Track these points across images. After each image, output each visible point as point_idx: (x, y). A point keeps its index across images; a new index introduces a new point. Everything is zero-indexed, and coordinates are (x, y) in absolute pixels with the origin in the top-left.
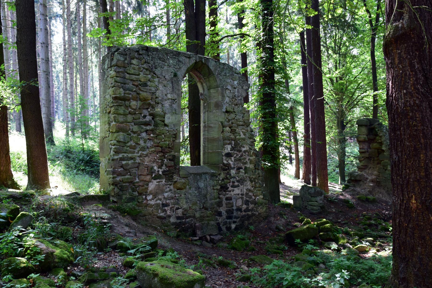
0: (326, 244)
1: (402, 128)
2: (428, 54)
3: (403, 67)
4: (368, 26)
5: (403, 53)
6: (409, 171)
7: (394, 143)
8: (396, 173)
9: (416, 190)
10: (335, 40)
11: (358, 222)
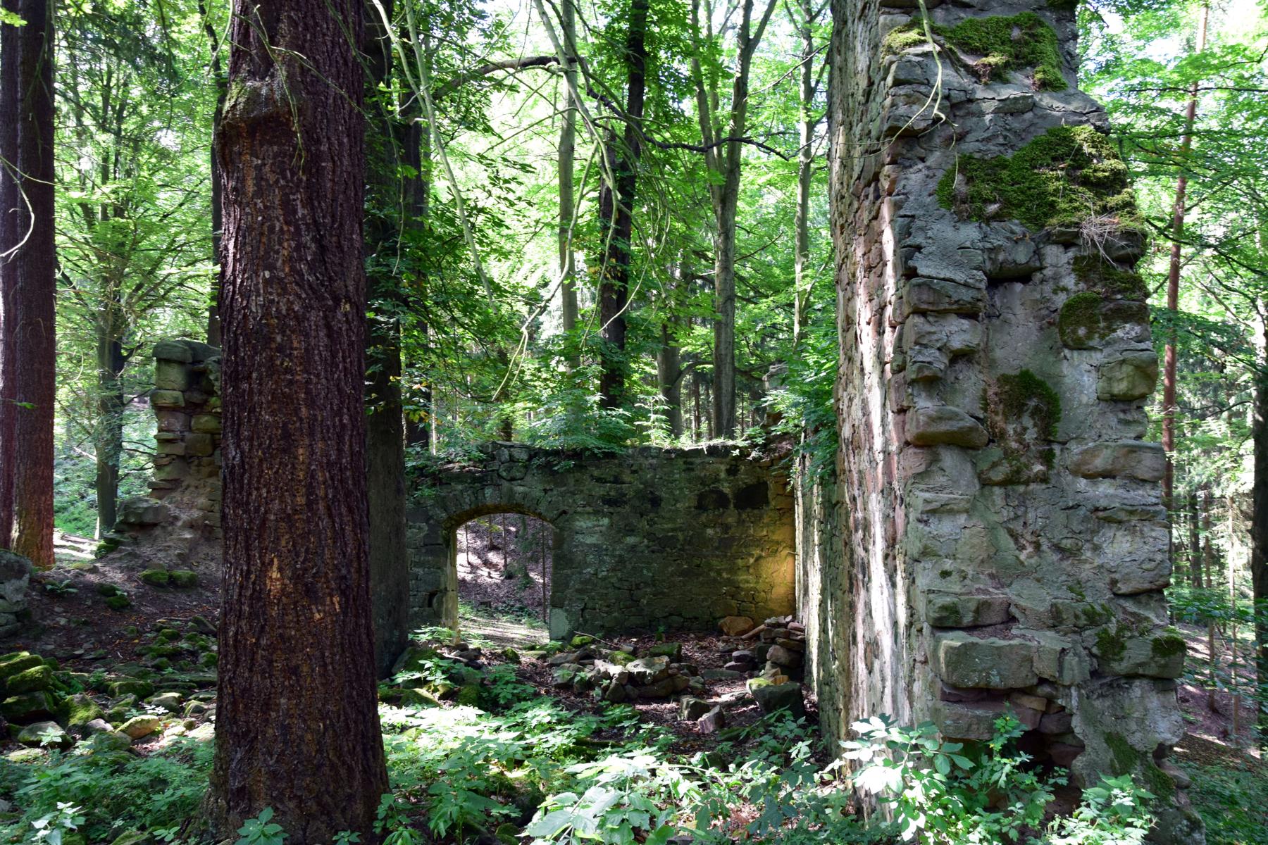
0: (24, 735)
1: (254, 375)
2: (329, 185)
3: (266, 207)
4: (207, 75)
5: (267, 168)
6: (268, 492)
7: (233, 413)
8: (233, 499)
9: (283, 543)
10: (107, 88)
11: (137, 649)
